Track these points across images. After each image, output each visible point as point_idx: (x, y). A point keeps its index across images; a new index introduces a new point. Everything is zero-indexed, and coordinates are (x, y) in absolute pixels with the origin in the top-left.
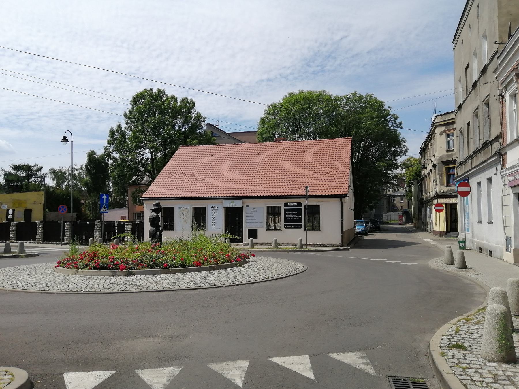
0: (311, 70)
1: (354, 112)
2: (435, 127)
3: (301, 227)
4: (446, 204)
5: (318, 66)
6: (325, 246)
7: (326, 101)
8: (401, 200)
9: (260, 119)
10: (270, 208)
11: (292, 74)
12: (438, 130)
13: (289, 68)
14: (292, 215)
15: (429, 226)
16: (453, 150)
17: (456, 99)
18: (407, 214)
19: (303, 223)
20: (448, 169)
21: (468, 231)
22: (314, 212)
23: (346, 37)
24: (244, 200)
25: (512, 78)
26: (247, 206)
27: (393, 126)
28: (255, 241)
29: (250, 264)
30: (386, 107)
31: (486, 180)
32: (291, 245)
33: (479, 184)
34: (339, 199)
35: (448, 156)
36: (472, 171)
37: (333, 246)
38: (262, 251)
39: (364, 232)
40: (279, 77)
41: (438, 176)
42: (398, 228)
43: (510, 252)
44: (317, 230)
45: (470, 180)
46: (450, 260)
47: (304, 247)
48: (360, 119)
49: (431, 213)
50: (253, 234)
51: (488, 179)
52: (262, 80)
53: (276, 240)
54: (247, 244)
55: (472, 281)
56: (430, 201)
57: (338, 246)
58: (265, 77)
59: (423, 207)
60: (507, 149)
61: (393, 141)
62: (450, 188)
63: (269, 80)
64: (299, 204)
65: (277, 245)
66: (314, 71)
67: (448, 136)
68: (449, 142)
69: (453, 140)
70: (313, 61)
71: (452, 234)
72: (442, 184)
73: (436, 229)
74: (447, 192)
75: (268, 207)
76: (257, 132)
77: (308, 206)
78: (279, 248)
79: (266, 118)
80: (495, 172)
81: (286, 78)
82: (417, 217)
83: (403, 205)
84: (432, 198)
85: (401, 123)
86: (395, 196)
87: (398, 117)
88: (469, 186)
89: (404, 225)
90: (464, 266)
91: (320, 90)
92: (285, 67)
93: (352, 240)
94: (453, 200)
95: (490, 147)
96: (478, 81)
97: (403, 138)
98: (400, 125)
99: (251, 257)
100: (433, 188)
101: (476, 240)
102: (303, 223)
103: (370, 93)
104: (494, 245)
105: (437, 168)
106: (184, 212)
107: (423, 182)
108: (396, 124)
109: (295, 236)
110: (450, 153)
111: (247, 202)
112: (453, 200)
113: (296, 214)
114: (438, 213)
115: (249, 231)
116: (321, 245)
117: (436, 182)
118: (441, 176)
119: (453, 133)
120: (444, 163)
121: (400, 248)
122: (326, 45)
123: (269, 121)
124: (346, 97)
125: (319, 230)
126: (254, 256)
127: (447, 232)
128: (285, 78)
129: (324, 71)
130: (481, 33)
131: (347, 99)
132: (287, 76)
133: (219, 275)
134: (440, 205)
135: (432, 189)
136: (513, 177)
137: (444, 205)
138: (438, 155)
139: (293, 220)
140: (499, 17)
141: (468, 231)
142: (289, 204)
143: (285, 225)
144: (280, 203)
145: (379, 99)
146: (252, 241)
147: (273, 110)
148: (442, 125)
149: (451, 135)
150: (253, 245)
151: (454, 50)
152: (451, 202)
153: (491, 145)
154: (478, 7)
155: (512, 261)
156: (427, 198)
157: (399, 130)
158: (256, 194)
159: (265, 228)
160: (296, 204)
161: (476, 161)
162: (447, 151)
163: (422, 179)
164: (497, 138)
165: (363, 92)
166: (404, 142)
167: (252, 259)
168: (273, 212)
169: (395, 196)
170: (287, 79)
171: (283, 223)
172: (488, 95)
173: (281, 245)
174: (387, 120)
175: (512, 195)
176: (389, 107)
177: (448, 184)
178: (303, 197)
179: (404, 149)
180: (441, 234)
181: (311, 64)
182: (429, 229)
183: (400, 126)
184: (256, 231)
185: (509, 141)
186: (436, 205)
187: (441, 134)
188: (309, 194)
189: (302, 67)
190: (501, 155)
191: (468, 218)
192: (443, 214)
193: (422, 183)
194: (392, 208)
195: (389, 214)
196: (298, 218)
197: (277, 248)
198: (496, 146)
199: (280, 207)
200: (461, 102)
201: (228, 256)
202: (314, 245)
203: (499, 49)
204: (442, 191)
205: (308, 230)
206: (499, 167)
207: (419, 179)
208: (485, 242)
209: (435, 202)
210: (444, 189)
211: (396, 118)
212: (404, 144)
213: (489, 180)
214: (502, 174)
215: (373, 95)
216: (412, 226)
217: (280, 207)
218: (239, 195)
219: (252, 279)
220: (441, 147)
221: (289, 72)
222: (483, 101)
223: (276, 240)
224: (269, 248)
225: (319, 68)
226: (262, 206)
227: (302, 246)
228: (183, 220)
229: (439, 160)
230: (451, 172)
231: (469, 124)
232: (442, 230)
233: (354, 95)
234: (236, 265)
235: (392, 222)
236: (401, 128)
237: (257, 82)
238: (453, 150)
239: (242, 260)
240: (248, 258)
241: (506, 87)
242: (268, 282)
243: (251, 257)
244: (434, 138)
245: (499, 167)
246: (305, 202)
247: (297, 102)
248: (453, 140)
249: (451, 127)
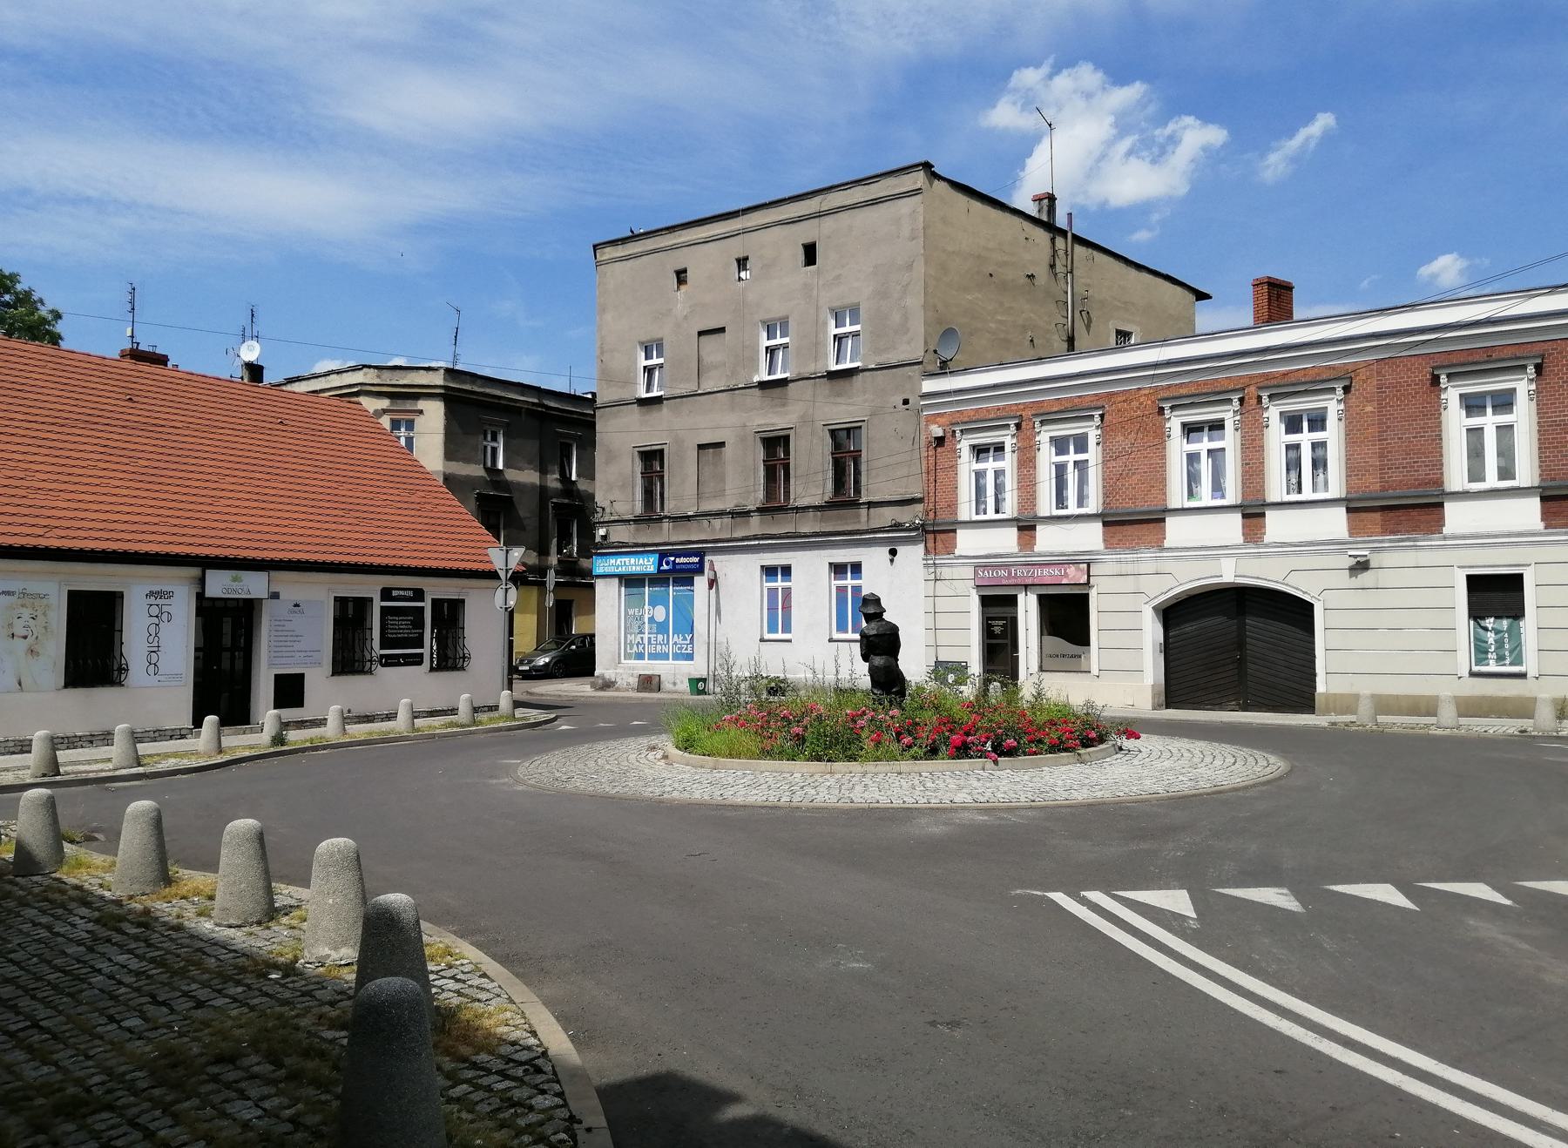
3: (420, 663)
10: (351, 605)
14: (402, 627)
22: (449, 616)
44: (593, 644)
50: (290, 691)
102: (426, 651)
106: (26, 613)
142: (395, 593)
143: (382, 656)
144: (368, 588)
160: (411, 594)
168: (350, 616)
171: (377, 650)
184: (300, 678)
196: (414, 633)
228: (21, 645)
249: (409, 405)
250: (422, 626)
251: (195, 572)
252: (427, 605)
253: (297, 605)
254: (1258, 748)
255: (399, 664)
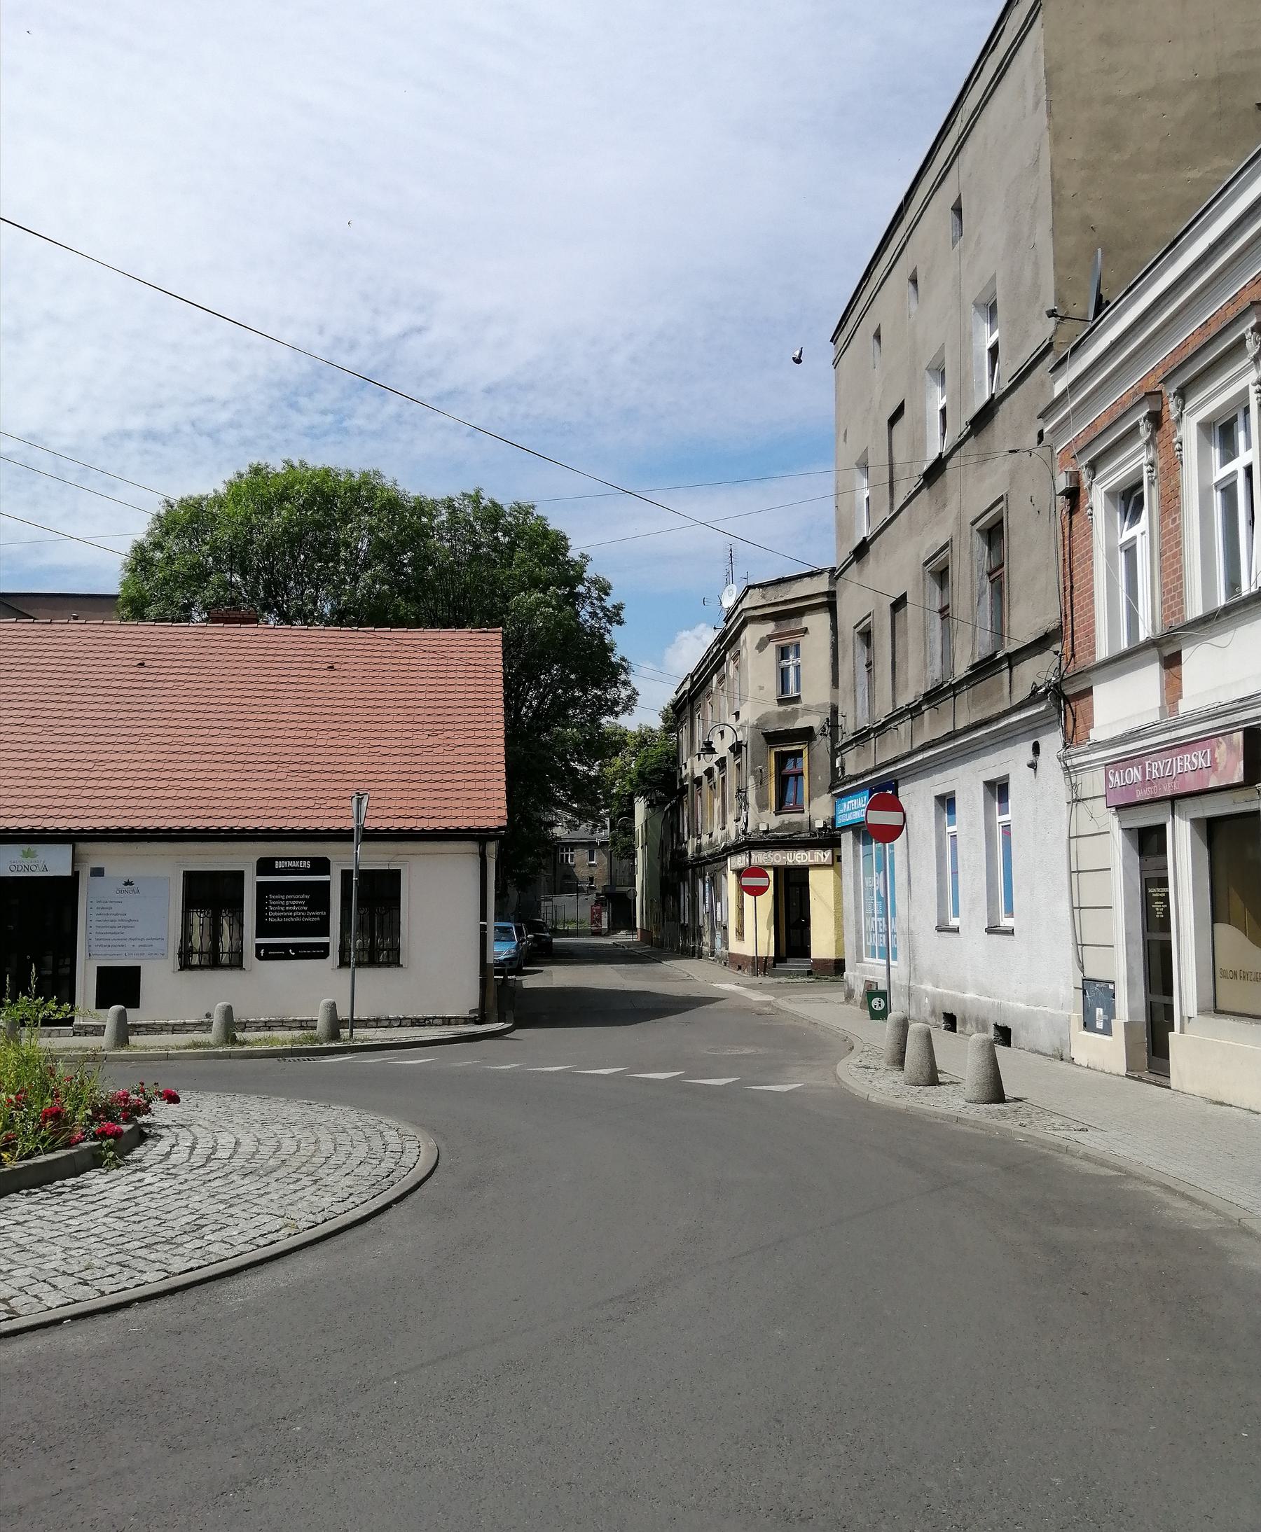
0: (300, 421)
1: (474, 557)
2: (744, 624)
3: (325, 955)
4: (776, 869)
5: (324, 412)
6: (417, 1022)
7: (383, 507)
8: (591, 859)
9: (127, 549)
11: (233, 424)
12: (752, 634)
13: (225, 404)
14: (293, 909)
15: (707, 939)
16: (796, 699)
17: (843, 525)
18: (617, 905)
19: (333, 939)
20: (782, 759)
21: (895, 959)
22: (378, 897)
23: (419, 330)
24: (83, 847)
25: (1136, 426)
26: (98, 872)
27: (594, 615)
28: (133, 1016)
29: (163, 1147)
30: (573, 554)
31: (981, 786)
32: (283, 1024)
33: (947, 802)
34: (472, 847)
35: (782, 717)
36: (920, 757)
37: (447, 1021)
38: (168, 1057)
39: (515, 966)
40: (187, 429)
41: (751, 781)
42: (589, 946)
43: (1107, 1031)
45: (900, 789)
46: (927, 1069)
47: (345, 1033)
48: (494, 582)
49: (718, 897)
50: (120, 986)
51: (989, 785)
52: (127, 435)
53: (228, 1012)
54: (98, 1031)
55: (1119, 1169)
56: (718, 860)
57: (466, 1021)
58: (136, 423)
59: (684, 878)
60: (1093, 676)
61: (597, 667)
62: (787, 818)
63: (150, 435)
64: (321, 865)
65: (231, 1027)
66: (312, 427)
67: (783, 653)
68: (784, 673)
69: (797, 667)
70: (310, 395)
71: (793, 964)
72: (762, 806)
73: (745, 948)
74: (778, 830)
75: (190, 878)
76: (116, 597)
77: (363, 874)
78: (243, 1043)
79: (158, 546)
80: (1030, 757)
81: (213, 435)
82: (657, 909)
83: (595, 871)
84: (726, 849)
85: (619, 608)
86: (573, 845)
87: (610, 587)
88: (899, 808)
89: (606, 935)
90: (997, 1095)
91: (366, 468)
92: (210, 400)
93: (506, 1002)
94: (798, 858)
95: (1006, 673)
96: (950, 456)
97: (623, 659)
98: (618, 615)
99: (158, 1105)
100: (731, 817)
101: (928, 987)
102: (333, 939)
103: (525, 502)
104: (1022, 1006)
105: (747, 755)
107: (687, 798)
108: (603, 608)
109: (306, 989)
110: (789, 708)
111: (97, 854)
112: (798, 858)
113: (308, 903)
114: (748, 899)
115: (105, 975)
116: (401, 1022)
117: (745, 798)
118: (761, 782)
119: (797, 646)
120: (773, 738)
121: (671, 1018)
122: (353, 346)
123: (170, 560)
124: (449, 504)
125: (396, 963)
126: (173, 1099)
127: (779, 958)
128: (210, 435)
129: (346, 431)
130: (972, 290)
131: (453, 511)
132: (218, 431)
133: (17, 1235)
134: (758, 871)
135: (716, 824)
136: (1136, 773)
137: (771, 873)
138: (749, 715)
139: (293, 924)
140: (1057, 231)
141: (895, 959)
142: (278, 865)
143: (259, 947)
145: (553, 525)
146: (122, 1016)
147: (187, 521)
148: (764, 618)
149: (792, 649)
150: (124, 1032)
151: (836, 363)
152: (790, 862)
153: (1011, 668)
154: (957, 210)
155: (1123, 1072)
156: (699, 848)
157: (615, 628)
158: (135, 823)
159: (173, 960)
160: (307, 865)
161: (932, 726)
162: (781, 702)
163: (684, 790)
164: (1042, 643)
165: (504, 493)
166: (626, 671)
167: (162, 1113)
168: (209, 895)
169: (573, 845)
170: (217, 442)
172: (1001, 499)
173: (244, 1026)
174: (578, 596)
175: (1118, 835)
176: (583, 556)
177: (781, 807)
178: (343, 836)
179: (624, 693)
180: (760, 966)
181: (303, 401)
182: (706, 949)
183: (615, 616)
185: (1102, 653)
186: (739, 873)
187: (761, 646)
188: (371, 824)
189: (271, 407)
190: (1064, 700)
191: (894, 915)
192: (766, 901)
193: (680, 801)
194: (567, 883)
195: (563, 900)
196: (314, 917)
197: (234, 1041)
198: (1035, 672)
199: (239, 876)
200: (865, 532)
201: (56, 1115)
202: (377, 1023)
203: (1058, 340)
204: (763, 827)
205: (359, 964)
206: (1052, 742)
207: (667, 786)
208: (970, 995)
209: (740, 861)
210: (770, 821)
211: (605, 590)
212: (623, 677)
213: (998, 790)
214: (1069, 763)
215: (533, 507)
216: (636, 938)
217: (239, 876)
218: (62, 824)
219: (222, 1248)
220: (761, 688)
221: (224, 416)
222: (973, 523)
223: (228, 1012)
224: (196, 1045)
225: (329, 418)
226: (165, 871)
227: (335, 1026)
229: (756, 727)
230: (790, 767)
231: (899, 604)
232: (762, 953)
233: (476, 499)
234: (95, 1161)
235: (571, 927)
236: (620, 623)
237: (105, 439)
238: (796, 699)
239: (118, 1133)
240: (147, 1111)
241: (1093, 466)
242: (308, 1263)
243: (158, 1105)
244: (734, 659)
245: (1052, 742)
246: (342, 858)
247: (283, 497)
248: (797, 667)
249: (793, 625)
250: (326, 907)
251: (67, 849)
252: (335, 880)
253: (127, 883)
254: (387, 1110)
255: (287, 957)
